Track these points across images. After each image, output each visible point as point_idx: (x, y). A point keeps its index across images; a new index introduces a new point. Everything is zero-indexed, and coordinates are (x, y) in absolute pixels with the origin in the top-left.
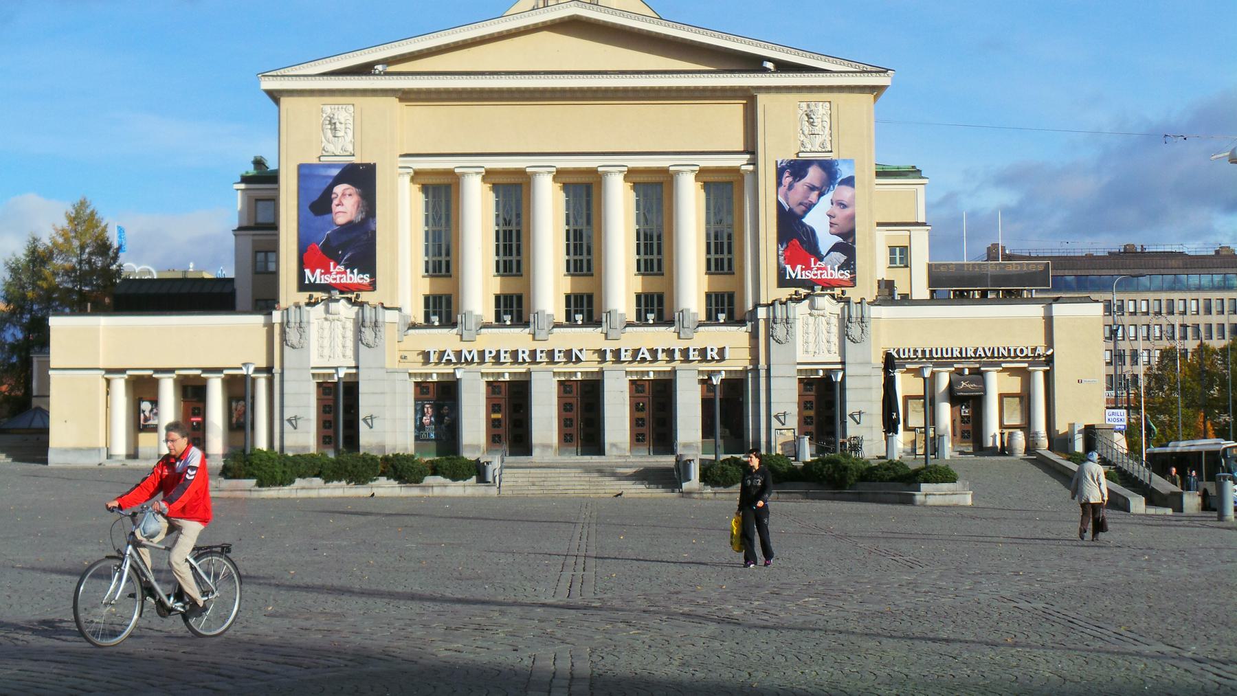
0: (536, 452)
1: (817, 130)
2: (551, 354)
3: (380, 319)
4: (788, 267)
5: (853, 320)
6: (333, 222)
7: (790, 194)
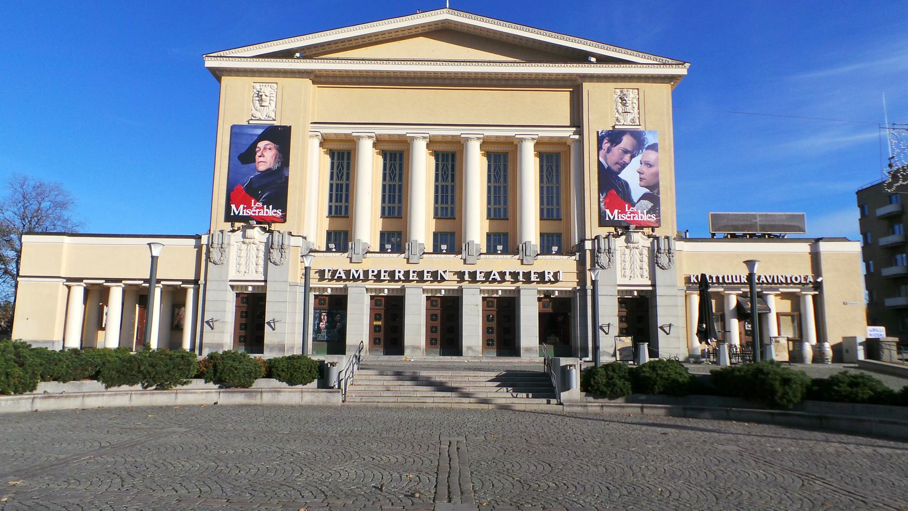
0: (407, 352)
1: (629, 109)
2: (421, 274)
3: (286, 243)
4: (608, 211)
6: (255, 169)
7: (608, 156)
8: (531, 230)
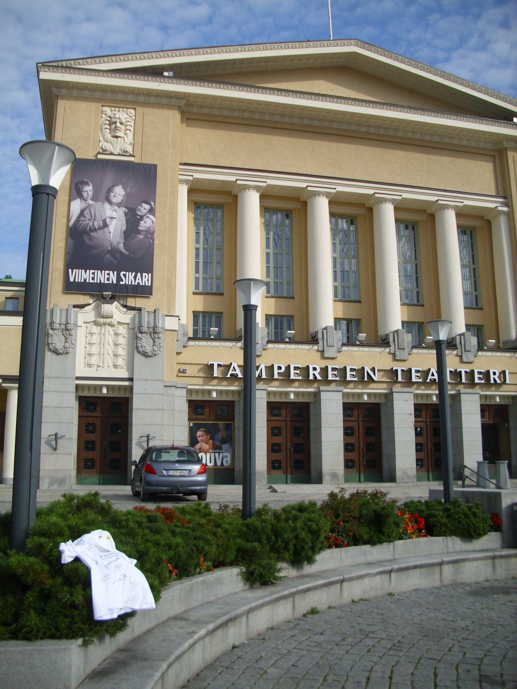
5: (57, 326)
8: (327, 310)
